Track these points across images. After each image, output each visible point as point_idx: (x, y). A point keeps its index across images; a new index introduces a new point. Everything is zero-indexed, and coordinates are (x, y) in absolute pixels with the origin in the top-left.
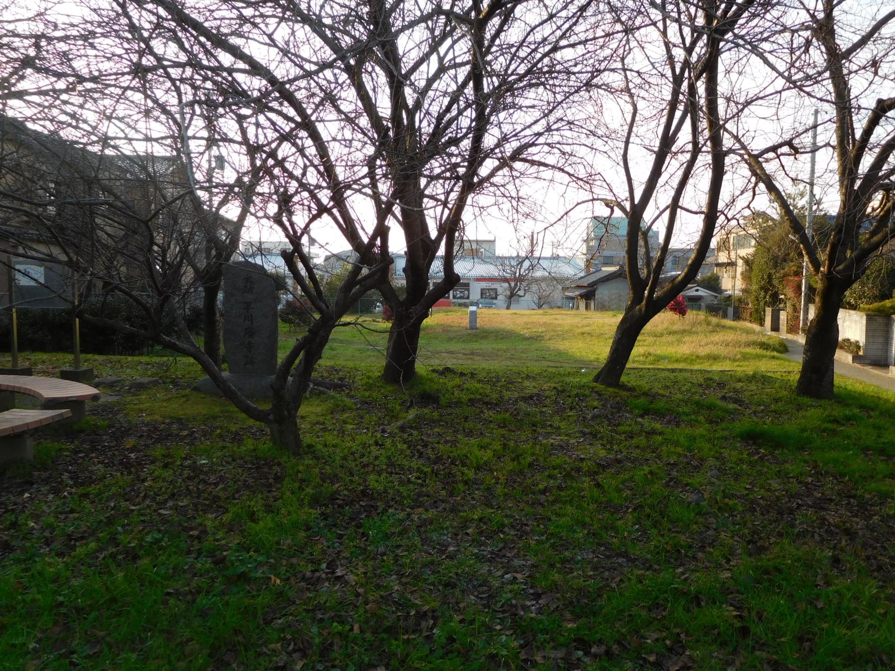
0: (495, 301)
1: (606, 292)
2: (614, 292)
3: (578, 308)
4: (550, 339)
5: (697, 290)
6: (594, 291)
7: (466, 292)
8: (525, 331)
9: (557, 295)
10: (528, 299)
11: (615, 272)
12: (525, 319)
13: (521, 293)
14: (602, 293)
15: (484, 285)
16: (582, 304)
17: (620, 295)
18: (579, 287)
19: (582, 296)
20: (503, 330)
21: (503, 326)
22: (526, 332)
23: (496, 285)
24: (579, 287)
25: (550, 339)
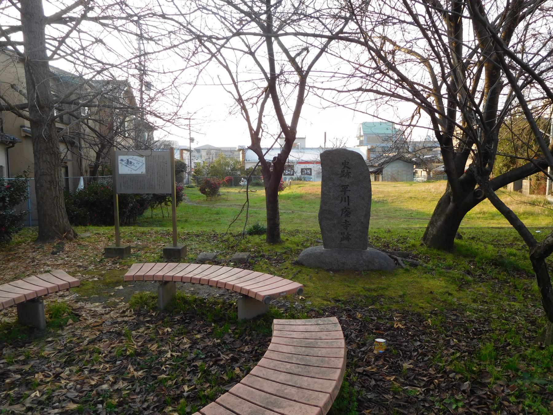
2: (394, 169)
15: (303, 166)
17: (398, 171)
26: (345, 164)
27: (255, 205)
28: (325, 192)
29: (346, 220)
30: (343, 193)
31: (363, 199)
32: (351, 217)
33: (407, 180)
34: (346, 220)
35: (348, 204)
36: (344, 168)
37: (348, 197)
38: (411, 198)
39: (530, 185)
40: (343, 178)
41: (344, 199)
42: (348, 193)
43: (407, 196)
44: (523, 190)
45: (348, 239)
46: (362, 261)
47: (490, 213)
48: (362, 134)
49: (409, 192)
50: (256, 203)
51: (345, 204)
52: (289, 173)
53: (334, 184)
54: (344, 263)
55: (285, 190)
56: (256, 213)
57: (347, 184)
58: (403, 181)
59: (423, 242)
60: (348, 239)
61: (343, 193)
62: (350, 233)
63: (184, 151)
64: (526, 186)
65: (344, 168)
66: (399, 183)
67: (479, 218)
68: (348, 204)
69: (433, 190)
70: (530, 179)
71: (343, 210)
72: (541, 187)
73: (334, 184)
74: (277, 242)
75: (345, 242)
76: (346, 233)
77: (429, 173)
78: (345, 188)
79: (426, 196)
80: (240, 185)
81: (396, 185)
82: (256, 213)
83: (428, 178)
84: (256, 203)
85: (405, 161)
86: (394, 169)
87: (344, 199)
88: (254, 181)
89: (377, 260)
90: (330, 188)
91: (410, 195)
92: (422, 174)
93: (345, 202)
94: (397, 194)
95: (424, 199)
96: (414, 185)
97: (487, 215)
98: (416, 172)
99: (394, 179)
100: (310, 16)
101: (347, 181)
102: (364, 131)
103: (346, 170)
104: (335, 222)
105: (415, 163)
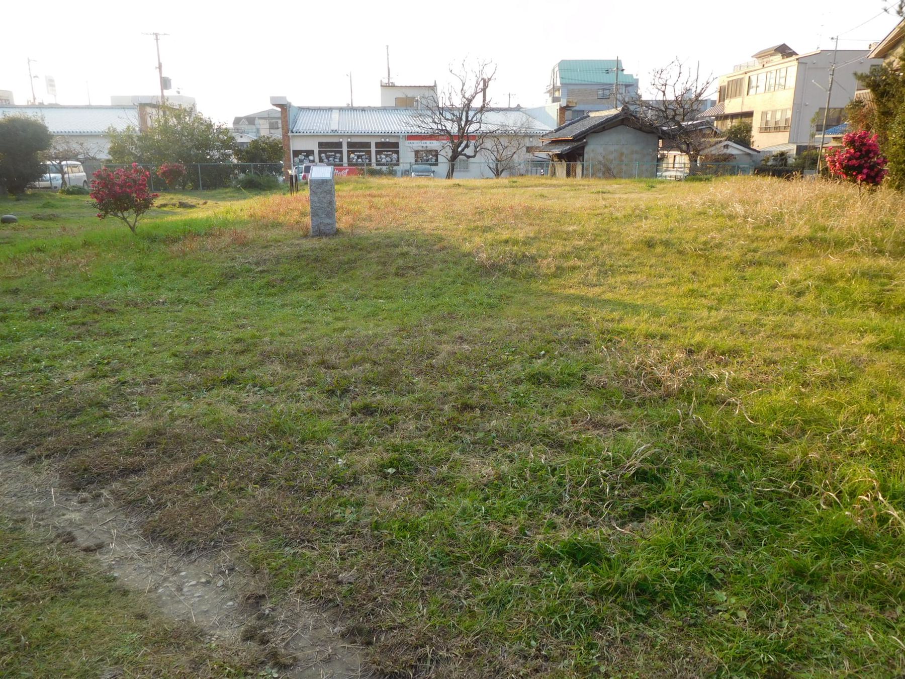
0: (433, 168)
1: (600, 150)
2: (612, 148)
3: (554, 174)
4: (560, 272)
5: (726, 146)
6: (583, 148)
7: (395, 156)
8: (478, 240)
9: (521, 157)
10: (482, 161)
11: (616, 116)
12: (477, 199)
13: (469, 151)
14: (595, 150)
15: (418, 145)
16: (561, 168)
17: (622, 154)
18: (555, 142)
19: (560, 157)
20: (411, 239)
21: (413, 223)
22: (477, 245)
23: (434, 145)
24: (555, 142)
25: (560, 272)
33: (640, 176)
38: (650, 244)
43: (633, 233)
48: (558, 84)
49: (643, 215)
58: (630, 176)
63: (149, 110)
66: (618, 180)
69: (739, 209)
77: (693, 159)
79: (718, 238)
81: (608, 188)
83: (691, 169)
85: (640, 129)
86: (612, 148)
91: (647, 228)
92: (677, 161)
94: (591, 226)
95: (707, 253)
96: (660, 186)
98: (664, 157)
99: (608, 173)
100: (851, 655)
102: (561, 78)
105: (664, 135)
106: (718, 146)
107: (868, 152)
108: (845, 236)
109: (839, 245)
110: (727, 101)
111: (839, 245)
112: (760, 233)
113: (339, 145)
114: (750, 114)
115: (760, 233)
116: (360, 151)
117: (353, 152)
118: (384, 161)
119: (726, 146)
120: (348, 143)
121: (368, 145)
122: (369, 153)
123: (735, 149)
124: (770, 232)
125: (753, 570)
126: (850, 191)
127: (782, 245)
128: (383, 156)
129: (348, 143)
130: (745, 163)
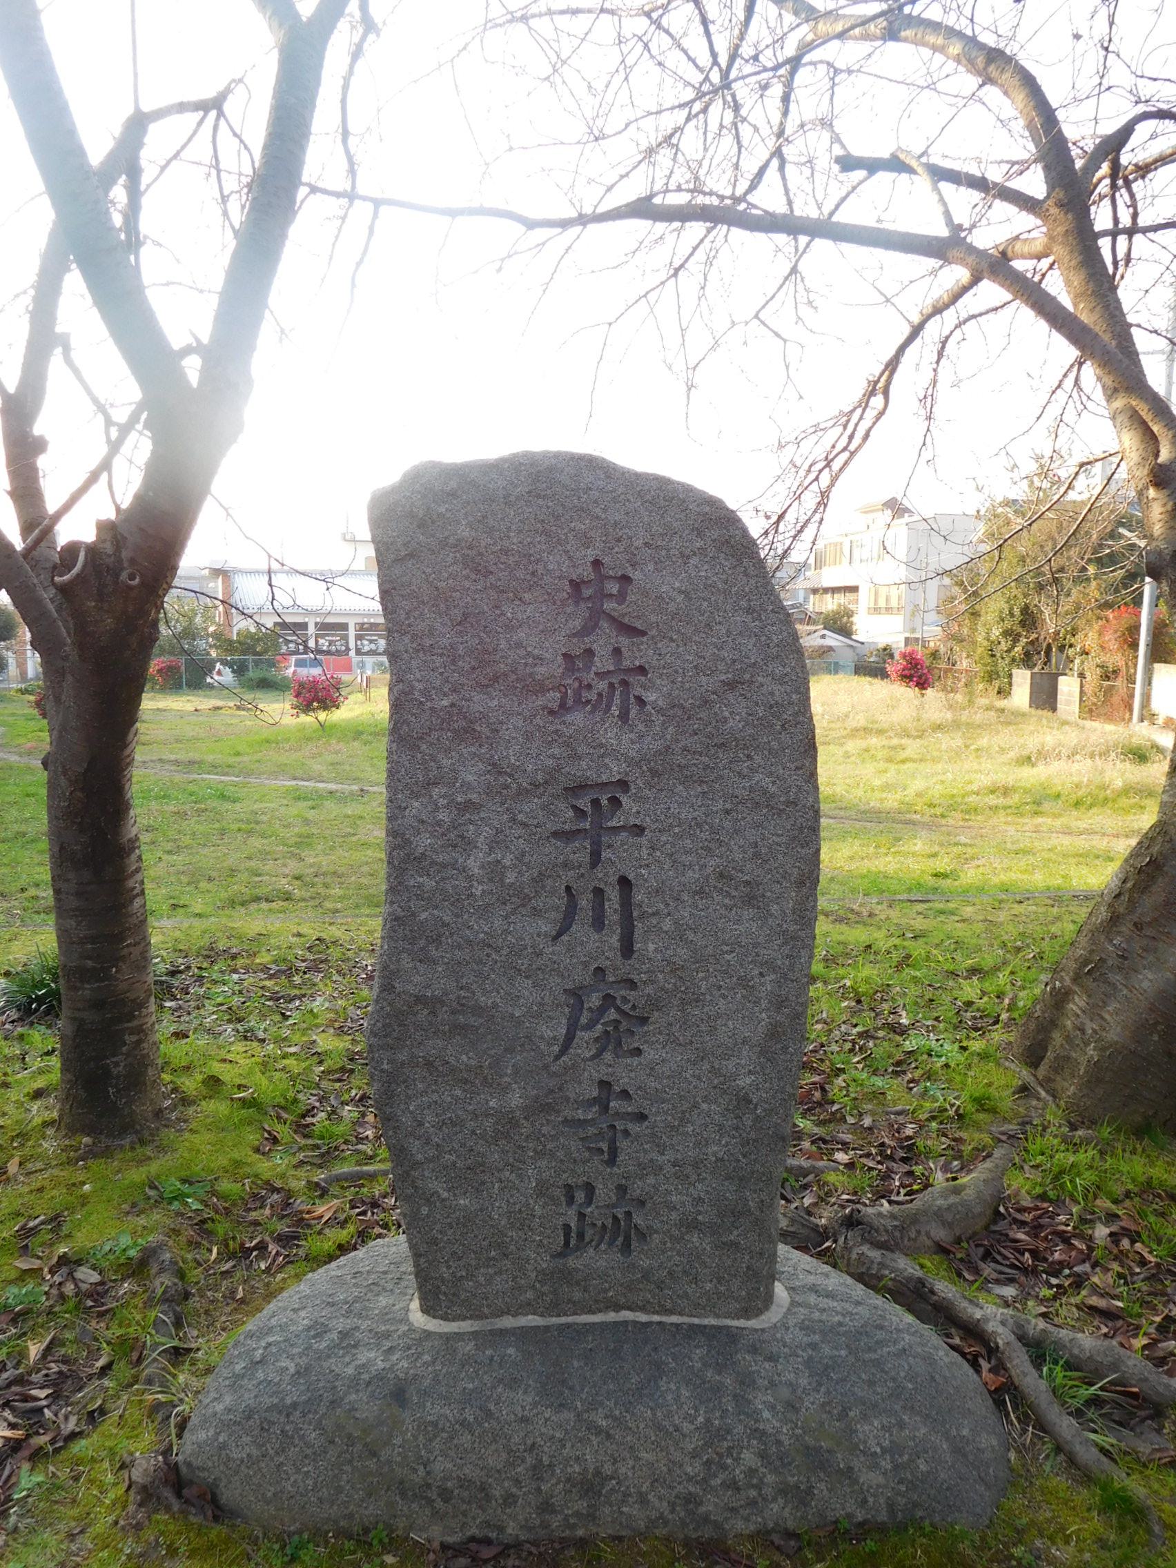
26: (598, 592)
27: (232, 760)
28: (423, 842)
29: (604, 1085)
30: (579, 852)
31: (749, 900)
32: (650, 1054)
34: (604, 1085)
35: (627, 949)
36: (588, 629)
37: (624, 882)
39: (1082, 692)
40: (577, 718)
41: (584, 902)
42: (621, 855)
44: (1060, 706)
45: (623, 1234)
46: (749, 1458)
47: (1026, 791)
50: (238, 754)
51: (594, 944)
52: (373, 647)
53: (496, 768)
54: (590, 1486)
55: (343, 708)
56: (223, 797)
57: (615, 770)
59: (1025, 1074)
60: (623, 1234)
61: (579, 852)
62: (638, 1188)
64: (1070, 694)
65: (588, 629)
67: (994, 809)
68: (627, 949)
70: (1082, 675)
71: (576, 995)
72: (1116, 699)
73: (496, 768)
74: (124, 1130)
75: (597, 1260)
76: (604, 1193)
78: (595, 809)
80: (210, 686)
82: (223, 797)
84: (238, 754)
87: (584, 902)
88: (252, 674)
89: (871, 1432)
90: (468, 806)
93: (599, 923)
97: (1015, 799)
101: (616, 746)
103: (603, 641)
104: (515, 1100)
106: (813, 636)
107: (917, 664)
108: (886, 726)
109: (880, 732)
110: (825, 569)
111: (880, 732)
112: (833, 725)
113: (304, 626)
114: (854, 589)
115: (833, 725)
116: (333, 635)
117: (323, 636)
118: (366, 649)
119: (823, 637)
120: (316, 624)
121: (344, 627)
122: (345, 638)
123: (833, 640)
124: (839, 725)
125: (1092, 1421)
126: (905, 693)
127: (845, 733)
128: (366, 642)
129: (316, 624)
130: (847, 658)
